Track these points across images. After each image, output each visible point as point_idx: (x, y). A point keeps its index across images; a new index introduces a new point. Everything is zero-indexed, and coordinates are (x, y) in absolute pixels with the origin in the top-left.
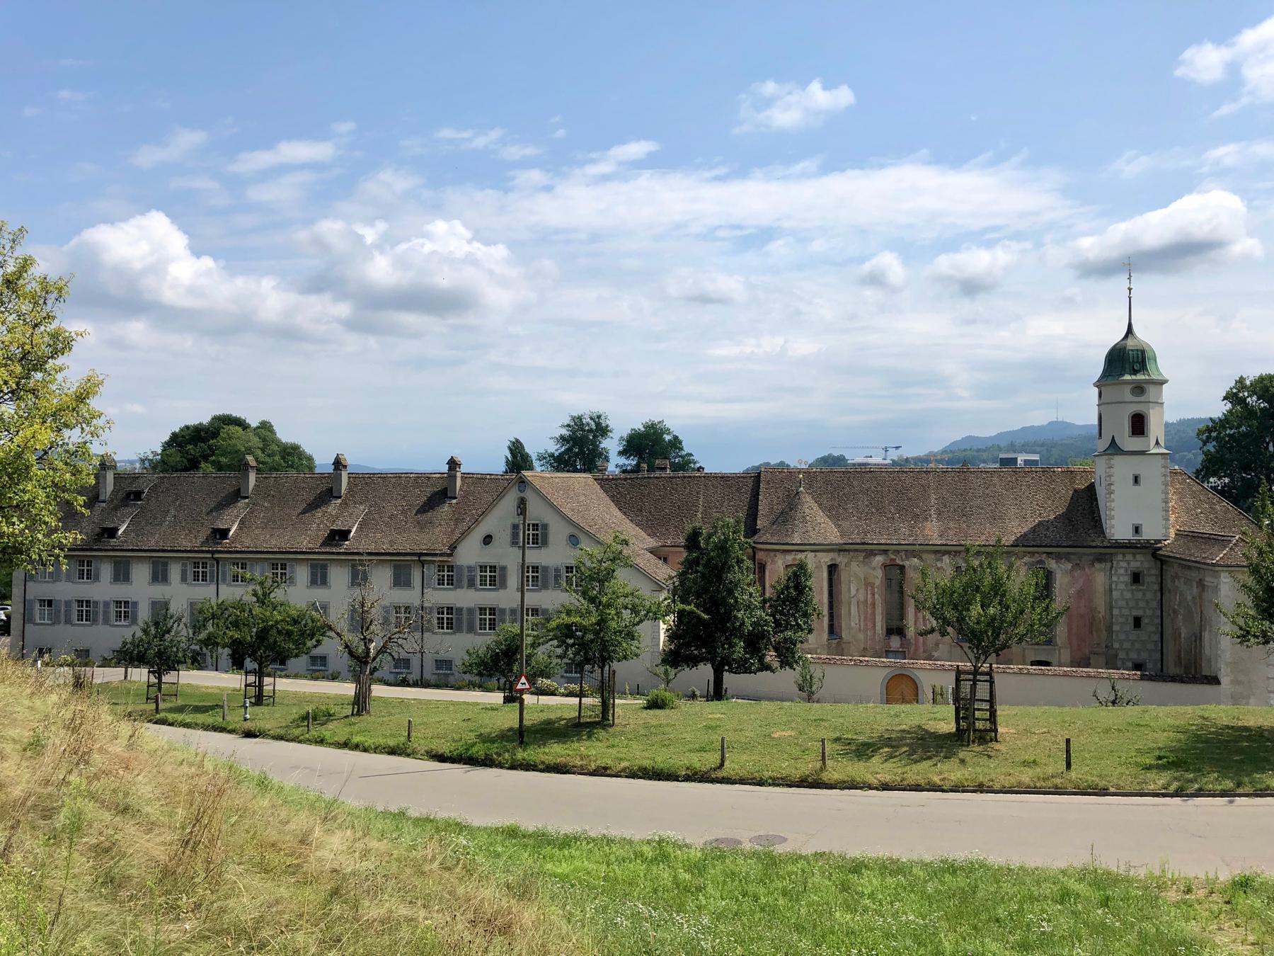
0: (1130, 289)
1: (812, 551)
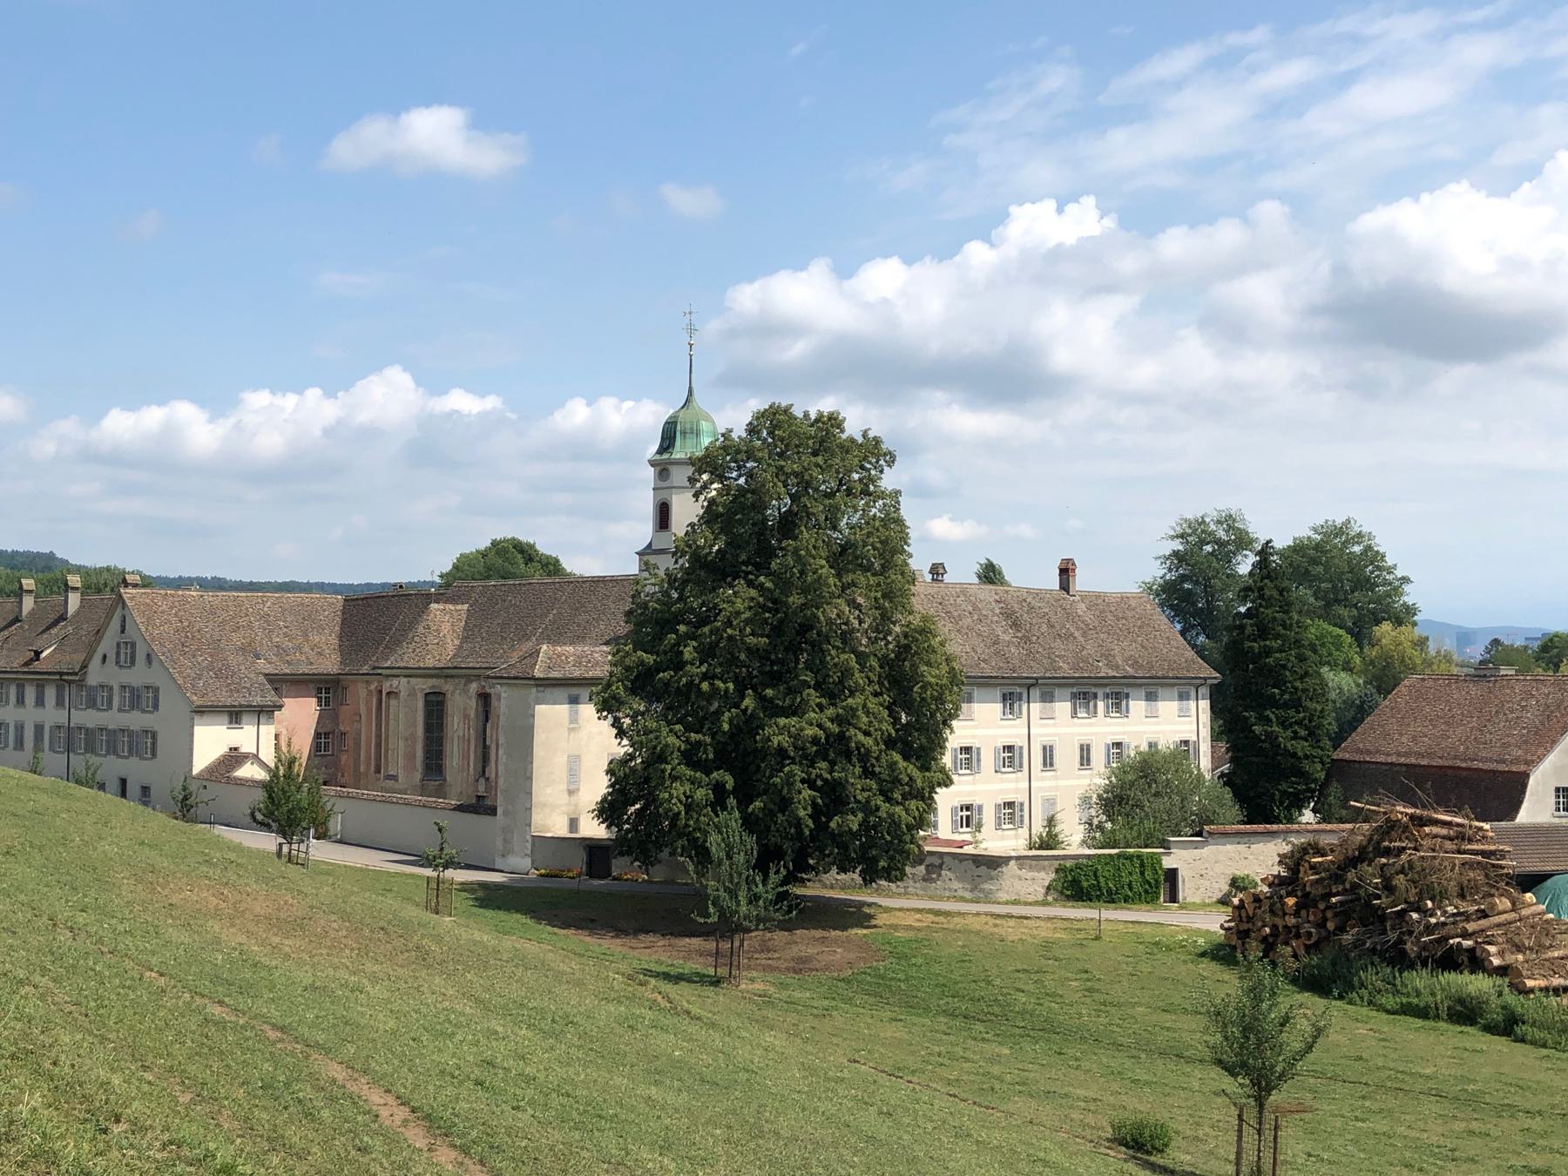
0: (691, 345)
1: (405, 676)
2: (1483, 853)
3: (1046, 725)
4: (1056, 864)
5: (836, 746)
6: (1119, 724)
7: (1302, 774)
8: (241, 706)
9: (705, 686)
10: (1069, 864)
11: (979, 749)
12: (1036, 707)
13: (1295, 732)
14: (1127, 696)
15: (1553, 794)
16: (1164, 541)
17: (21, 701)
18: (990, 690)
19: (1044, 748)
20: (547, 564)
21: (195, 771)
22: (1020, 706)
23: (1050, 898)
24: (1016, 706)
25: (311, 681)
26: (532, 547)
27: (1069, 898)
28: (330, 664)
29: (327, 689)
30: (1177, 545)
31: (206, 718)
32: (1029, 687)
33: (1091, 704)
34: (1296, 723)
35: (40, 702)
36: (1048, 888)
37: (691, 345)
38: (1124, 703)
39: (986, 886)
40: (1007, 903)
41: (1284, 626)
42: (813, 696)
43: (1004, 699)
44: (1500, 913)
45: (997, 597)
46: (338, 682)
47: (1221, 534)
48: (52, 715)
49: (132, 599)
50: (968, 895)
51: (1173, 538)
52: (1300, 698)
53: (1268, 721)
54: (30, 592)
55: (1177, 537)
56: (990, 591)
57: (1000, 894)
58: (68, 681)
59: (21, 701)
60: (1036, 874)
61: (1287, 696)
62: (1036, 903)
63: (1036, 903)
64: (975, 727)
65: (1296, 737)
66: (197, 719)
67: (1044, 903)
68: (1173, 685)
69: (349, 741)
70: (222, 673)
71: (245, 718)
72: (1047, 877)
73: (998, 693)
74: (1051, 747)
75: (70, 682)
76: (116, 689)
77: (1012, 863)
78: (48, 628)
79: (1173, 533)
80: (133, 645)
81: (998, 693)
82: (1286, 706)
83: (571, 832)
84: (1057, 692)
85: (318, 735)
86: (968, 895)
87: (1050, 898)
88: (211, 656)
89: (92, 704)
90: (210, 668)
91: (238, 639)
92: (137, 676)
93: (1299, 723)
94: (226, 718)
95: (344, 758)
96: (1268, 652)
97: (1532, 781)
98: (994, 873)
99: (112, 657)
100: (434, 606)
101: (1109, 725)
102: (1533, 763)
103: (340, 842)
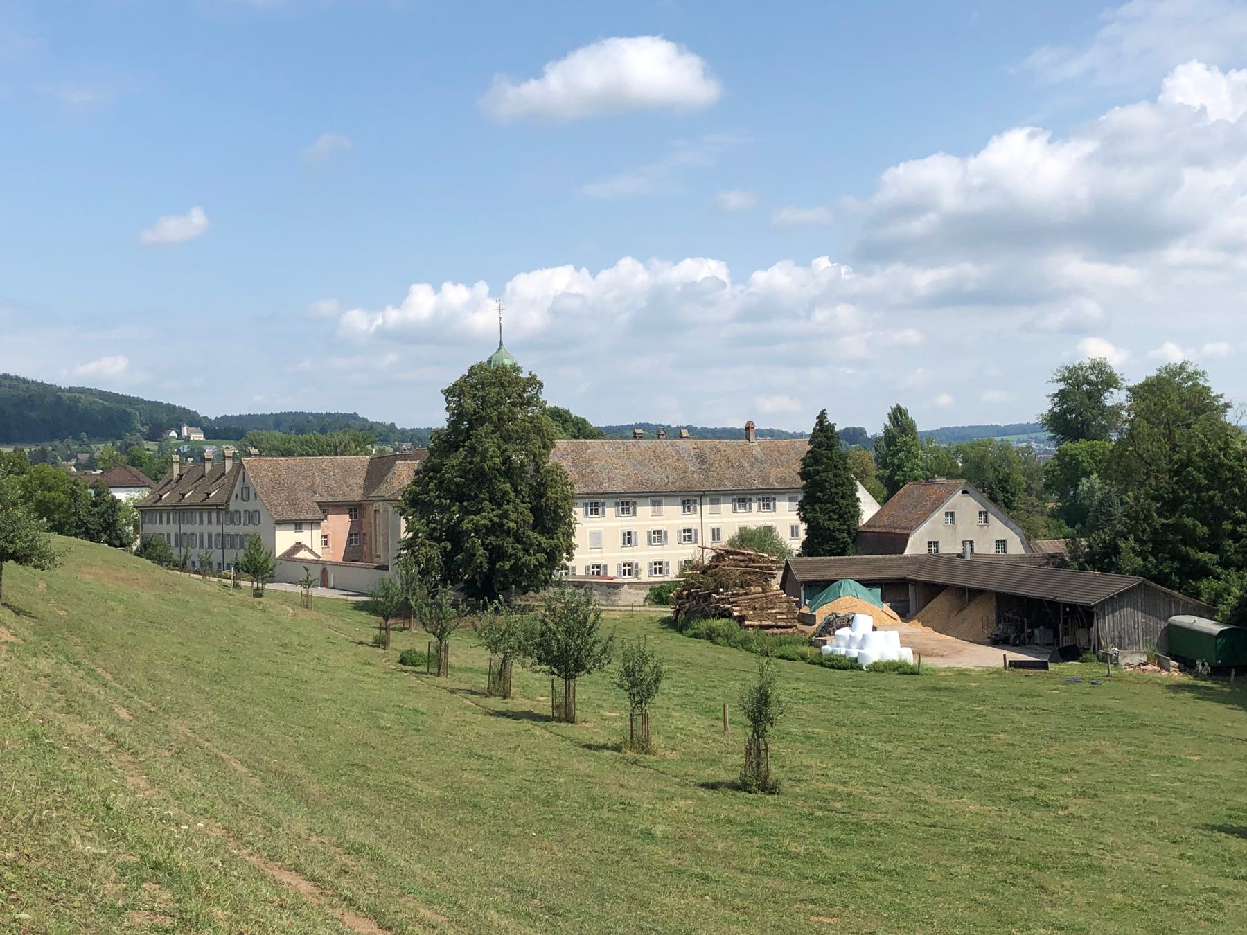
2: (761, 568)
3: (714, 518)
4: (650, 586)
5: (495, 528)
6: (768, 516)
7: (835, 539)
8: (301, 520)
9: (437, 501)
10: (657, 586)
11: (666, 532)
12: (707, 508)
13: (830, 517)
14: (774, 499)
15: (927, 545)
16: (1051, 384)
17: (201, 522)
18: (676, 499)
19: (713, 530)
20: (577, 424)
21: (277, 556)
22: (695, 508)
23: (647, 604)
24: (692, 507)
25: (345, 505)
26: (567, 412)
27: (657, 603)
28: (357, 496)
29: (355, 509)
30: (1062, 386)
31: (282, 527)
32: (701, 496)
33: (747, 505)
34: (831, 511)
35: (210, 522)
36: (646, 599)
37: (500, 318)
38: (772, 503)
39: (614, 598)
40: (624, 606)
41: (828, 458)
42: (487, 505)
43: (684, 503)
44: (753, 594)
45: (696, 447)
46: (361, 505)
47: (1093, 378)
48: (215, 529)
49: (247, 463)
50: (604, 603)
51: (1057, 381)
52: (834, 498)
53: (814, 510)
54: (177, 462)
55: (1060, 380)
56: (692, 443)
57: (620, 602)
58: (221, 509)
59: (201, 522)
60: (639, 592)
61: (826, 497)
62: (639, 606)
63: (639, 606)
64: (663, 519)
65: (830, 519)
66: (277, 527)
67: (644, 606)
68: (648, 497)
69: (367, 538)
70: (293, 502)
71: (304, 526)
72: (645, 593)
73: (680, 500)
74: (718, 530)
75: (222, 510)
76: (242, 513)
77: (626, 586)
78: (217, 480)
79: (1055, 377)
80: (249, 488)
81: (680, 500)
82: (826, 502)
83: (1010, 662)
84: (722, 499)
85: (350, 535)
86: (604, 603)
87: (647, 604)
88: (288, 492)
89: (232, 522)
90: (286, 500)
91: (305, 483)
92: (251, 506)
93: (833, 511)
94: (293, 526)
95: (365, 547)
96: (818, 472)
97: (911, 539)
98: (616, 591)
99: (240, 495)
100: (398, 462)
101: (760, 516)
102: (913, 529)
103: (333, 588)
